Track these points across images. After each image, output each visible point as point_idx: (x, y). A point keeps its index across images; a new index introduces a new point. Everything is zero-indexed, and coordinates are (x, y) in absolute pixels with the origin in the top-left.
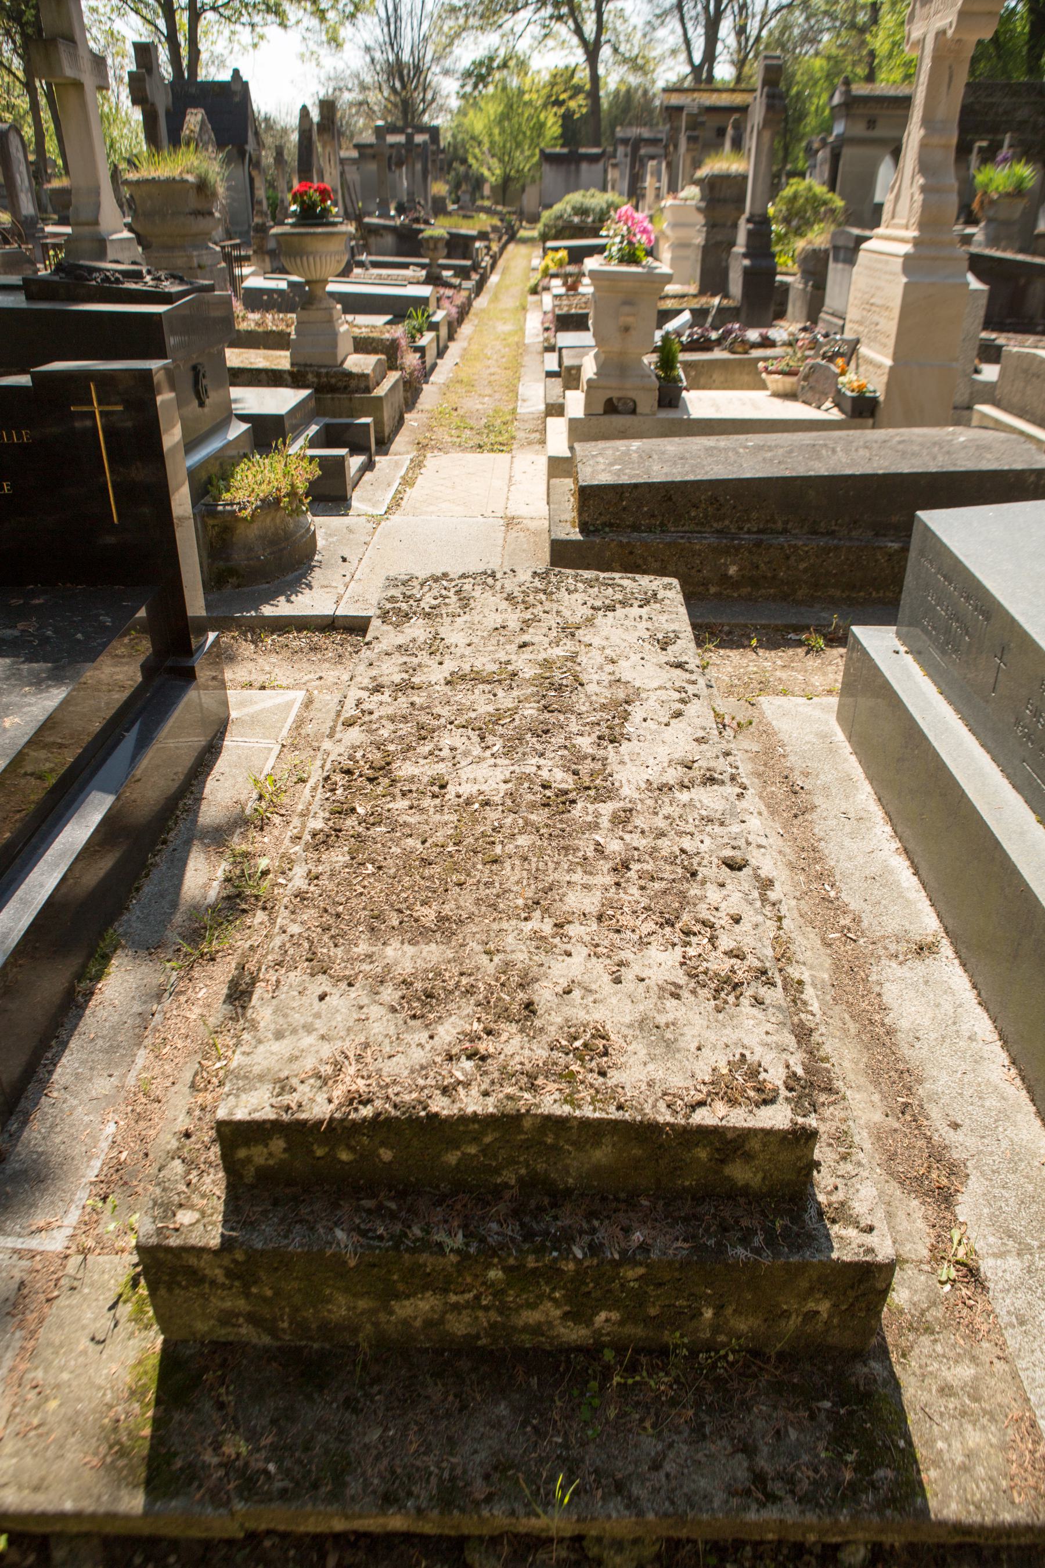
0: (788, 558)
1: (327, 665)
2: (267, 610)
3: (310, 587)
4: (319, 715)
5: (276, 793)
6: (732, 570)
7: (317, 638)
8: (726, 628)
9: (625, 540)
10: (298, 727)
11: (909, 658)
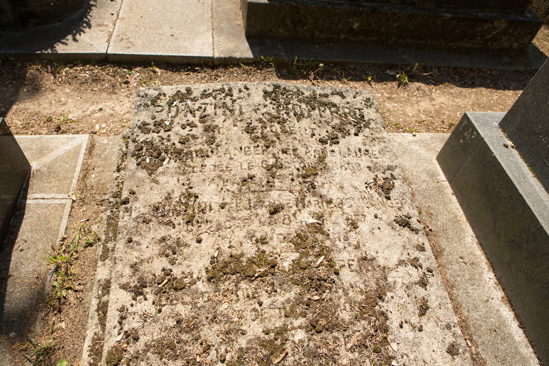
0: (388, 20)
1: (104, 95)
2: (60, 49)
3: (89, 26)
6: (356, 26)
7: (97, 70)
8: (352, 66)
9: (294, 5)
10: (85, 176)
11: (515, 152)
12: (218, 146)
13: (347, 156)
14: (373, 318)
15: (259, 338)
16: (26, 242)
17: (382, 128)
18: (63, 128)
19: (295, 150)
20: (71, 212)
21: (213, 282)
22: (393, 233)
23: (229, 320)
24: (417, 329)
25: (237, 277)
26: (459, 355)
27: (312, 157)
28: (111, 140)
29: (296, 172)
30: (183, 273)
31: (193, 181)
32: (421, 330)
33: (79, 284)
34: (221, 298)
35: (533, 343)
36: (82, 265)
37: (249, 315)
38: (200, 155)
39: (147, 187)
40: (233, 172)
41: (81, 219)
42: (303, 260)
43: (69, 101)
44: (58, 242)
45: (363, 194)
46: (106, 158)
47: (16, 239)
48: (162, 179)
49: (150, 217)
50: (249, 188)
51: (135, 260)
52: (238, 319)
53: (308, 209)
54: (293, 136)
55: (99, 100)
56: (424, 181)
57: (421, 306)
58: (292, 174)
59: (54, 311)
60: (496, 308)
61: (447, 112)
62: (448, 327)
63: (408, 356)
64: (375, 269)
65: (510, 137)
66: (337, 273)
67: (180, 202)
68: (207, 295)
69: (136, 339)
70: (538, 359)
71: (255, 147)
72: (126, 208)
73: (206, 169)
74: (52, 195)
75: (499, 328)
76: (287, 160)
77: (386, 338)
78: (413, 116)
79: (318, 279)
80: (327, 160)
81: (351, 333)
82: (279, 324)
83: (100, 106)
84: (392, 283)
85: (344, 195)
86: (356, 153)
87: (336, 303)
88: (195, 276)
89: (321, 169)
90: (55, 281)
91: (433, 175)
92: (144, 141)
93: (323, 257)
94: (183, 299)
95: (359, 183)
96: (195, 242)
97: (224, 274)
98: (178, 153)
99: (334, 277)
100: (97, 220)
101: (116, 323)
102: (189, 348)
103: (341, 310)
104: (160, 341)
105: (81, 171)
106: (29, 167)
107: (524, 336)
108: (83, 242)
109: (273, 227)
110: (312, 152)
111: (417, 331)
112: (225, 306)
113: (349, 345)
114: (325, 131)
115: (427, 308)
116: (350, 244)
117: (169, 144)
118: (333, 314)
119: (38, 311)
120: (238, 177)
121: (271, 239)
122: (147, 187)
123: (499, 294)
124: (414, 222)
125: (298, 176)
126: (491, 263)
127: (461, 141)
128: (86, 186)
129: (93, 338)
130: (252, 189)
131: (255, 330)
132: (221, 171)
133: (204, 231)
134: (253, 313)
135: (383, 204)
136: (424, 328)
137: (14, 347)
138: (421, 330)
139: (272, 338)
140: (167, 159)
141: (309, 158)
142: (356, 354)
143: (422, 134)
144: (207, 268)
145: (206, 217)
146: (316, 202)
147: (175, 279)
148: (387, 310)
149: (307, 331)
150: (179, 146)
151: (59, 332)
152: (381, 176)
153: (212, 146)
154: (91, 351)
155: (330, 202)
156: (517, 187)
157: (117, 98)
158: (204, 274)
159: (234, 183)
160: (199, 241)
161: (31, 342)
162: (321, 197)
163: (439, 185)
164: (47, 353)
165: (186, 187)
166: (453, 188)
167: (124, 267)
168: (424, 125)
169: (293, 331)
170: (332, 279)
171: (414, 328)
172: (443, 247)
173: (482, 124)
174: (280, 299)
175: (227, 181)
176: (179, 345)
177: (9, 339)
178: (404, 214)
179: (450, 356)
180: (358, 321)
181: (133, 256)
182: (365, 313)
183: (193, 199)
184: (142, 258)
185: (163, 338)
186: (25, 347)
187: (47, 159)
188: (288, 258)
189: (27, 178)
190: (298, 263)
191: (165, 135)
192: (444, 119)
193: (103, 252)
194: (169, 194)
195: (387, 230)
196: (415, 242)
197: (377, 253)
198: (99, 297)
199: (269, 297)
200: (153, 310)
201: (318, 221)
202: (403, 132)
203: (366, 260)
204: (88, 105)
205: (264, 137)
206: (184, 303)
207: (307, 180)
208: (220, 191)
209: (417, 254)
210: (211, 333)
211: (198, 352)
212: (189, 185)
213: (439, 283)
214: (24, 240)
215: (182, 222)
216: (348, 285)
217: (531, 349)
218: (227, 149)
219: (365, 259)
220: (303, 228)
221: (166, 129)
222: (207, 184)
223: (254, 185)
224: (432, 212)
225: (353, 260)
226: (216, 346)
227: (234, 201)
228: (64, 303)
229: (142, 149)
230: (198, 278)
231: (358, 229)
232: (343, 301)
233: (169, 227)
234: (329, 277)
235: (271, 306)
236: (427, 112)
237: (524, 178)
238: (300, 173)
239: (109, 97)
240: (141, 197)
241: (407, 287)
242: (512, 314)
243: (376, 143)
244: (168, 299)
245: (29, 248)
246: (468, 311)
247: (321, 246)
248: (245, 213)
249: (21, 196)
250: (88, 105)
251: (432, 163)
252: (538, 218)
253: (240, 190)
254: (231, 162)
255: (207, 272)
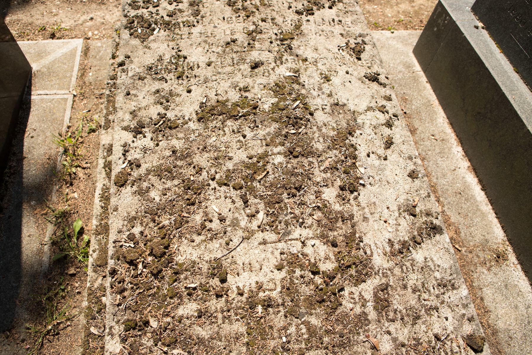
4: (95, 63)
5: (76, 146)
10: (83, 75)
11: (485, 33)
12: (203, 17)
13: (321, 25)
14: (344, 149)
15: (244, 162)
16: (35, 130)
17: (355, 3)
18: (57, 35)
19: (273, 19)
20: (73, 104)
21: (203, 122)
22: (362, 86)
23: (217, 149)
24: (382, 158)
25: (223, 118)
26: (419, 179)
27: (289, 25)
28: (104, 43)
29: (274, 37)
30: (176, 116)
31: (181, 45)
32: (385, 159)
33: (87, 163)
34: (210, 133)
35: (492, 201)
36: (87, 148)
37: (235, 145)
38: (186, 25)
39: (141, 53)
40: (217, 38)
41: (83, 110)
42: (282, 103)
43: (60, 12)
44: (64, 129)
45: (336, 55)
46: (101, 59)
47: (26, 128)
48: (153, 45)
49: (145, 75)
50: (232, 50)
51: (134, 108)
52: (225, 149)
53: (286, 65)
54: (271, 8)
55: (89, 11)
56: (400, 72)
57: (386, 141)
58: (271, 38)
59: (66, 184)
60: (462, 175)
61: (426, 13)
62: (410, 158)
63: (373, 177)
64: (345, 113)
65: (480, 19)
66: (312, 114)
67: (171, 62)
68: (198, 132)
69: (139, 166)
70: (496, 213)
71: (236, 17)
72: (123, 69)
73: (192, 36)
74: (55, 91)
75: (463, 191)
76: (266, 27)
77: (354, 163)
78: (393, 17)
79: (295, 118)
80: (302, 28)
81: (324, 158)
82: (261, 151)
83: (91, 16)
84: (361, 124)
85: (318, 55)
86: (330, 23)
87: (311, 137)
88: (186, 118)
89: (297, 35)
90: (64, 161)
91: (409, 66)
92: (135, 15)
93: (299, 101)
94: (177, 135)
95: (332, 47)
96: (185, 92)
97: (212, 115)
98: (168, 24)
99: (309, 117)
100: (97, 111)
101: (121, 155)
102: (184, 171)
103: (315, 142)
104: (159, 167)
105: (79, 70)
106: (31, 68)
107: (485, 196)
108: (87, 129)
109: (254, 78)
110: (289, 22)
111: (383, 160)
112: (214, 139)
113: (322, 168)
114: (301, 4)
115: (392, 143)
116: (323, 93)
117: (158, 17)
118: (308, 144)
119: (52, 184)
120: (222, 41)
121: (253, 87)
122: (141, 53)
123: (466, 164)
124: (382, 78)
125: (276, 40)
126: (459, 139)
127: (435, 29)
128: (85, 83)
129: (102, 188)
130: (235, 50)
131: (240, 156)
132: (207, 37)
133: (193, 83)
134: (238, 143)
135: (354, 63)
136: (388, 158)
137: (35, 212)
138: (385, 159)
139: (255, 161)
140: (158, 29)
141: (286, 26)
142: (329, 175)
143: (400, 31)
144: (197, 111)
145: (194, 73)
146: (292, 60)
147: (169, 120)
148: (356, 144)
149: (286, 156)
150: (167, 19)
151: (73, 200)
152: (352, 42)
153: (197, 17)
154: (101, 197)
155: (306, 60)
156: (484, 61)
157: (107, 9)
158: (195, 116)
159: (218, 46)
160: (189, 91)
161: (50, 208)
162: (297, 56)
163: (414, 74)
164: (65, 217)
165: (175, 51)
166: (427, 77)
167: (124, 114)
168: (403, 24)
169: (273, 156)
170: (307, 119)
171: (380, 157)
172: (416, 127)
173: (455, 9)
174: (261, 132)
175: (212, 44)
176: (175, 169)
177: (31, 206)
178: (373, 71)
179: (411, 179)
180: (330, 150)
181: (132, 105)
182: (336, 145)
183: (182, 59)
184: (140, 106)
185: (161, 165)
186: (45, 212)
187: (46, 61)
188: (268, 102)
189: (29, 78)
190: (277, 106)
191: (154, 10)
192: (423, 19)
193: (105, 123)
194: (160, 56)
195: (357, 84)
196: (383, 94)
197: (348, 100)
198: (105, 158)
199: (252, 131)
200: (152, 144)
201: (294, 75)
202: (382, 30)
203: (338, 105)
204: (79, 15)
205: (245, 9)
206: (178, 139)
207: (284, 43)
208: (206, 53)
209: (384, 103)
210: (202, 160)
211: (192, 173)
212: (178, 48)
213: (404, 125)
214: (33, 129)
215: (173, 77)
216: (322, 124)
217: (490, 207)
218: (211, 20)
219: (337, 104)
220: (281, 80)
221: (155, 5)
222: (194, 48)
223: (237, 47)
224: (407, 98)
225: (326, 105)
226: (207, 169)
227: (219, 60)
228: (74, 178)
229: (133, 22)
230: (189, 119)
231: (331, 82)
232: (317, 135)
233: (162, 82)
234: (305, 117)
235: (254, 138)
236: (406, 13)
237: (491, 54)
238: (278, 37)
239: (98, 7)
240: (136, 60)
241: (375, 127)
242: (476, 180)
243: (349, 15)
244: (164, 135)
245: (39, 136)
246: (437, 179)
247: (298, 93)
248: (229, 69)
249: (25, 93)
250: (79, 15)
251: (408, 56)
252: (501, 86)
253: (224, 51)
254: (215, 30)
255: (197, 114)
